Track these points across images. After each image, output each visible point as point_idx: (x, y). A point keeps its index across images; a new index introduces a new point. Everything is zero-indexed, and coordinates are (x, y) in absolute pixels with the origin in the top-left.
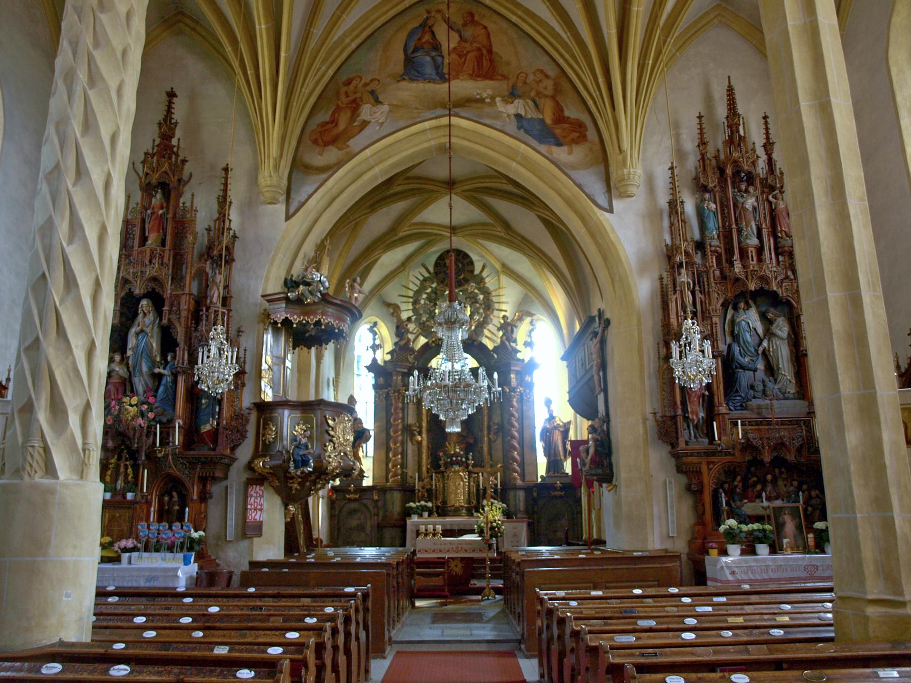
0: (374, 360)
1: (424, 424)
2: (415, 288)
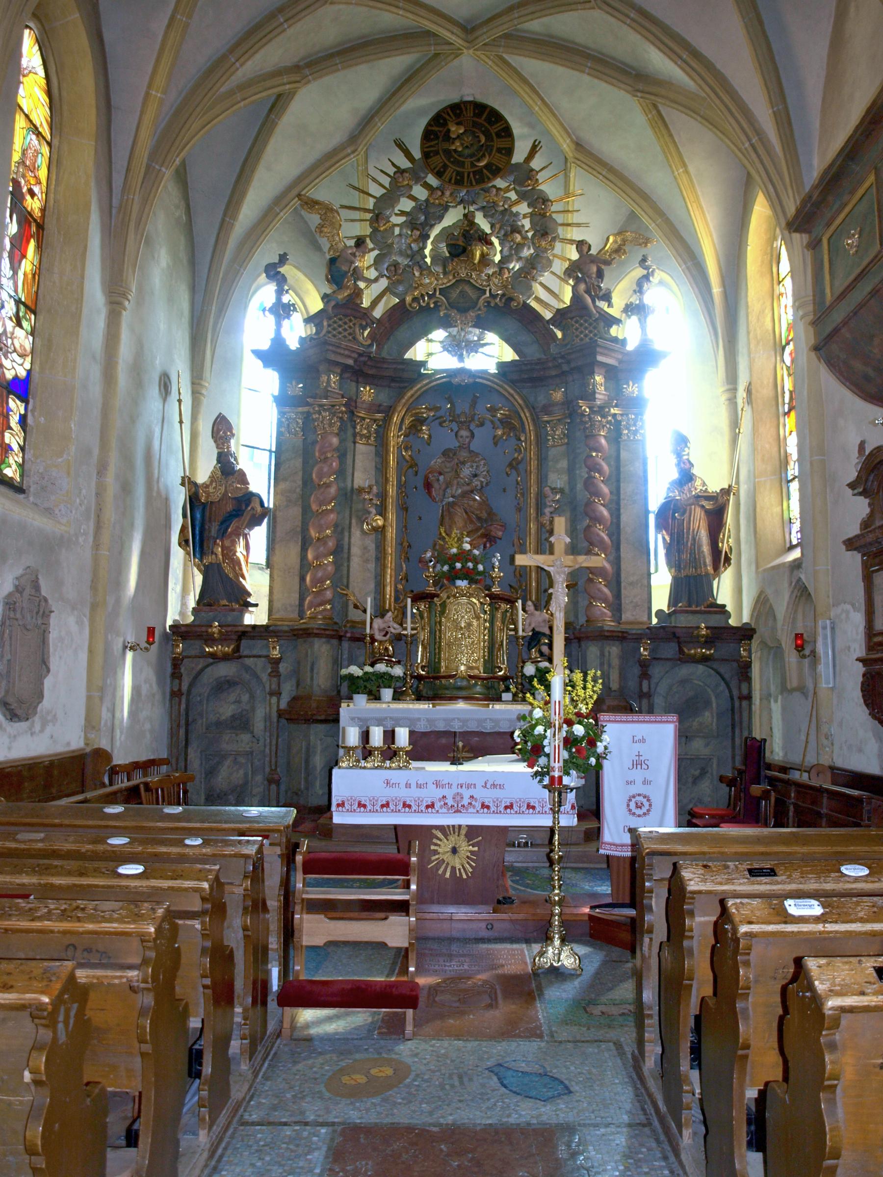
0: (278, 342)
1: (392, 491)
2: (377, 191)
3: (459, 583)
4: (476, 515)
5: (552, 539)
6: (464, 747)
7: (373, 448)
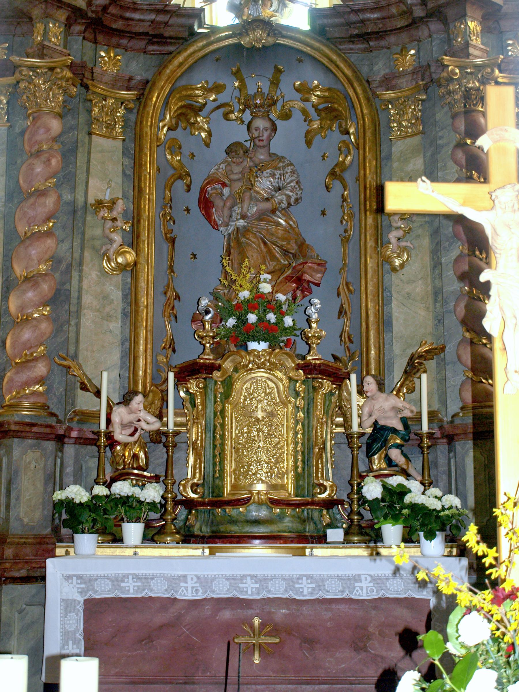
3: (253, 345)
4: (281, 247)
5: (483, 141)
6: (262, 625)
7: (119, 144)
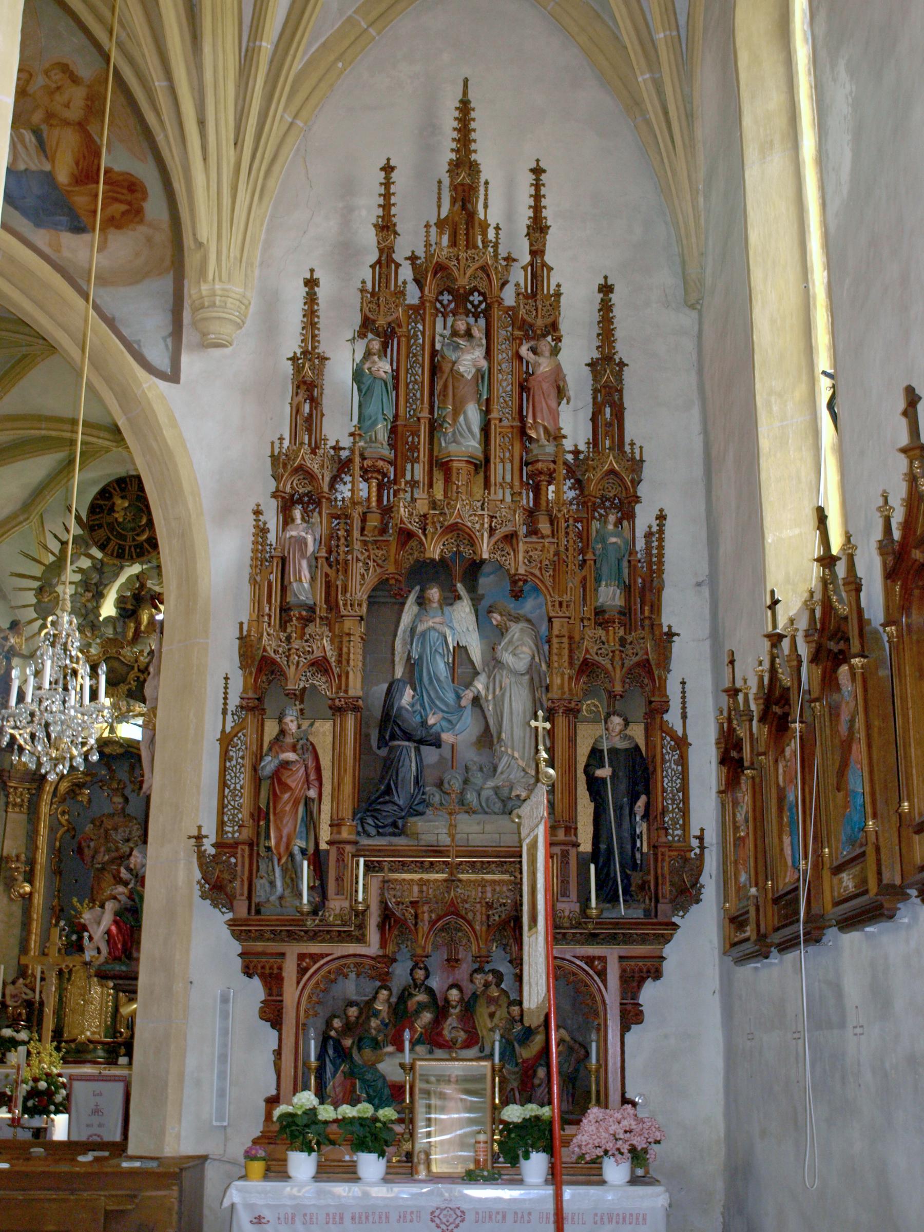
1: (42, 857)
